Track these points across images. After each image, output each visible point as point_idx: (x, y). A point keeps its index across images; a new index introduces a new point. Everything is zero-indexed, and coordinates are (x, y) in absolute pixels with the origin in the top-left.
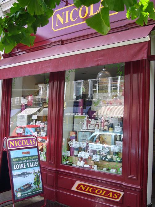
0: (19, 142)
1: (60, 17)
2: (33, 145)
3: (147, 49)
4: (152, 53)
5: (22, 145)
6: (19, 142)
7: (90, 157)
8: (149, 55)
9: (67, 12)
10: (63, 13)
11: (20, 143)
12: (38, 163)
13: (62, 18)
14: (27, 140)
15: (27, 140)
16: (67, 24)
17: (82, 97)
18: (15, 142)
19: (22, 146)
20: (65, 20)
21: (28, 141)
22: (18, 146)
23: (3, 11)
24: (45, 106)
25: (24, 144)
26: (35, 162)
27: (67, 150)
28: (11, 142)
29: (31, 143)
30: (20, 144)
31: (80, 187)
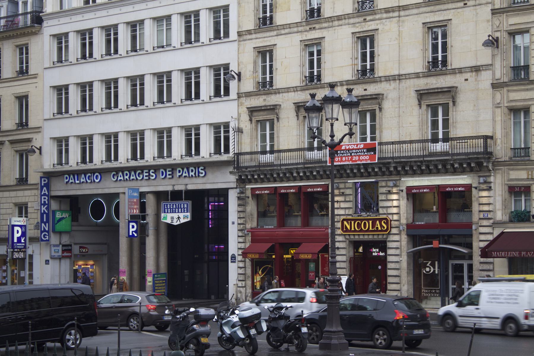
0: (358, 223)
2: (381, 231)
3: (486, 243)
5: (362, 228)
7: (513, 214)
9: (353, 222)
11: (359, 225)
15: (371, 222)
16: (353, 231)
17: (312, 8)
19: (361, 230)
21: (372, 222)
22: (355, 231)
23: (491, 72)
24: (354, 342)
28: (345, 223)
29: (379, 226)
30: (358, 228)
31: (380, 161)
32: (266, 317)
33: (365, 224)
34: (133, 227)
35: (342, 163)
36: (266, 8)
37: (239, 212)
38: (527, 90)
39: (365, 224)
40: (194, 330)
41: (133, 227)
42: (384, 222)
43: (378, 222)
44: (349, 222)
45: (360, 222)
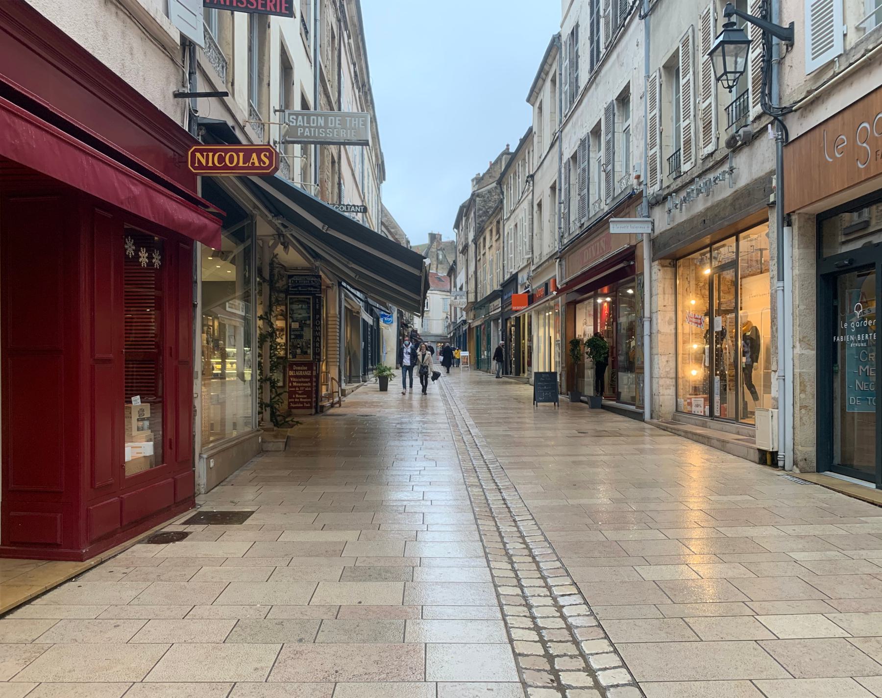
1: (796, 31)
4: (608, 694)
5: (226, 163)
6: (220, 157)
8: (570, 334)
9: (211, 154)
10: (205, 154)
12: (426, 307)
13: (876, 25)
14: (241, 154)
15: (241, 154)
18: (208, 156)
19: (226, 167)
20: (207, 162)
25: (231, 161)
26: (311, 382)
27: (635, 178)
28: (198, 155)
32: (229, 381)
33: (231, 158)
34: (301, 130)
35: (327, 81)
36: (491, 189)
37: (421, 410)
38: (592, 240)
39: (231, 158)
40: (466, 330)
41: (301, 130)
42: (265, 155)
43: (254, 155)
44: (205, 154)
45: (223, 154)
